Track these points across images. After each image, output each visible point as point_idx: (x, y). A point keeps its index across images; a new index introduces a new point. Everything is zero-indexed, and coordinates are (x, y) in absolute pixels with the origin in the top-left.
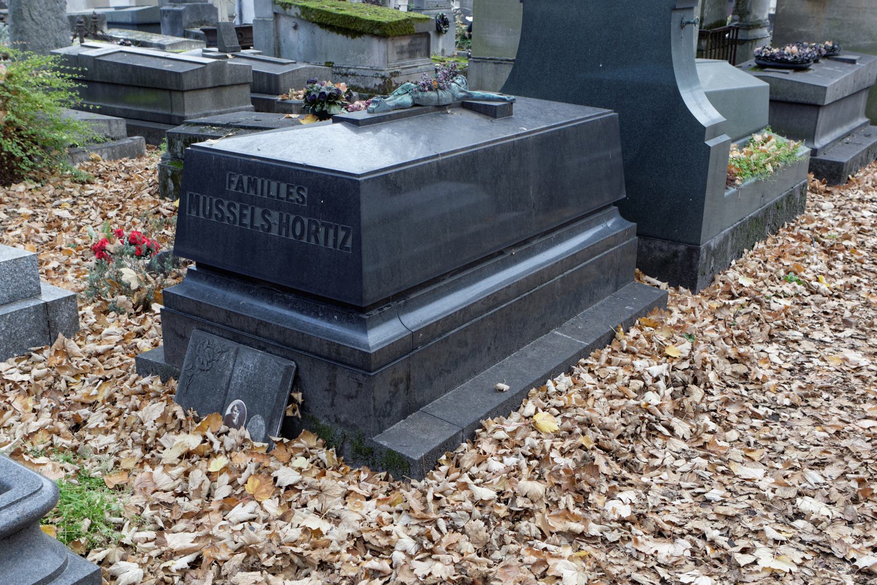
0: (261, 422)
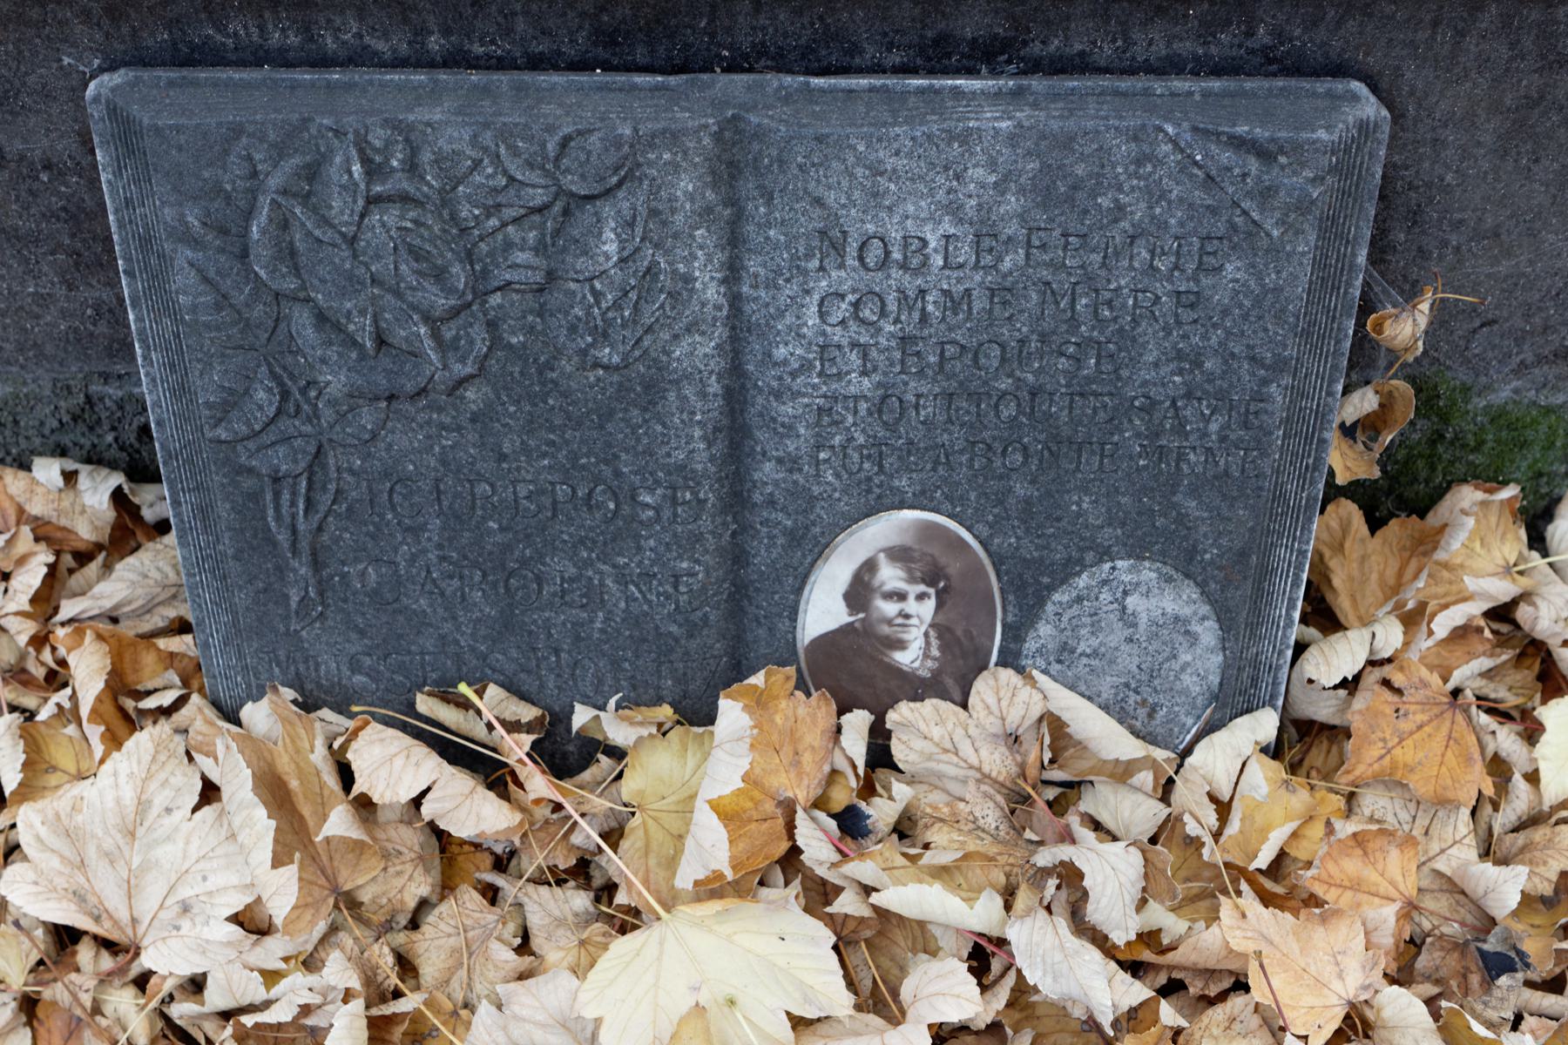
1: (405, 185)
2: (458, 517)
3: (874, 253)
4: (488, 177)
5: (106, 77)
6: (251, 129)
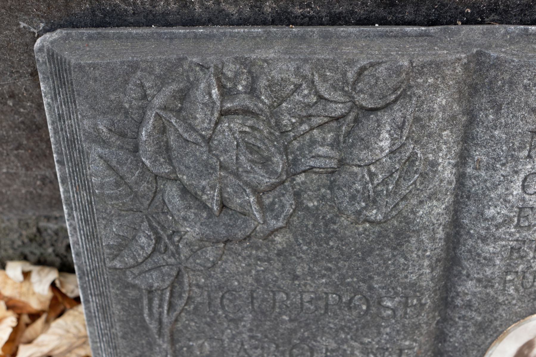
1: (247, 103)
2: (263, 313)
4: (305, 96)
5: (48, 35)
6: (143, 65)
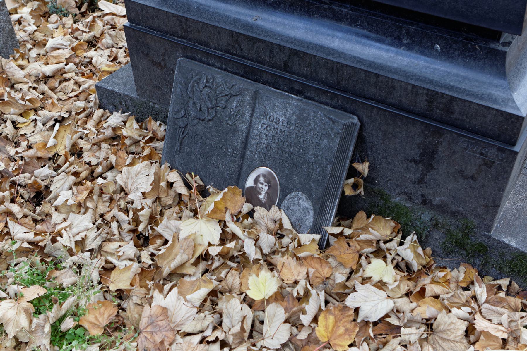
0: (306, 204)
3: (271, 119)
